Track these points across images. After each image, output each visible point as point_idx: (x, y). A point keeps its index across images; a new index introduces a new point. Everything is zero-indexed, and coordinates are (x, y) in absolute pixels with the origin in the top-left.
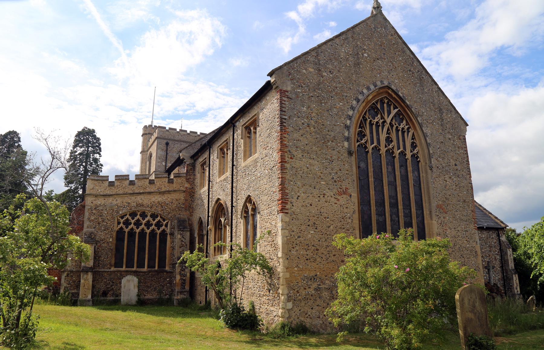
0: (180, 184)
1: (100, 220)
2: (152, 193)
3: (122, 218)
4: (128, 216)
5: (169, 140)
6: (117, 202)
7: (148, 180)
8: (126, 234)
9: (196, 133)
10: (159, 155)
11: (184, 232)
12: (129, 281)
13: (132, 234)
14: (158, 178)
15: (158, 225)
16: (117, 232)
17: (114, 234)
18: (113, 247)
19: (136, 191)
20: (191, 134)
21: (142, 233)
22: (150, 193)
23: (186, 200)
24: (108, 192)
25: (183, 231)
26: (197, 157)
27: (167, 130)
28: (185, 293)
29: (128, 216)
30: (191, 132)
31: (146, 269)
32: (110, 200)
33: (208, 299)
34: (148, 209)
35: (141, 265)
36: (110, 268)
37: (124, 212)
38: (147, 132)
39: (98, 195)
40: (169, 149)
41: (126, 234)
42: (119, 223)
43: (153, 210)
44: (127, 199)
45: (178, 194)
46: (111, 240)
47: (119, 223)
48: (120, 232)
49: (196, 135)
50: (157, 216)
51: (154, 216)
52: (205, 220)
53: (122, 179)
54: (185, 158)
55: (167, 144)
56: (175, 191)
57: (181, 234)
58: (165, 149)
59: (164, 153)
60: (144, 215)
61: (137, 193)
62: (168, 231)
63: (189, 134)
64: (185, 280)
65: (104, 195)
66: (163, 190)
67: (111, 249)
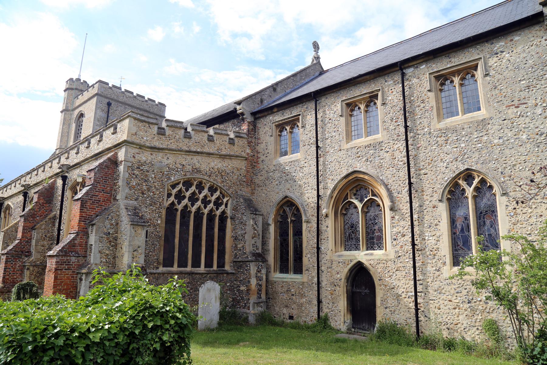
0: (241, 148)
1: (145, 188)
2: (212, 154)
3: (173, 186)
4: (181, 186)
5: (112, 99)
6: (169, 162)
7: (206, 134)
8: (179, 213)
9: (143, 97)
10: (97, 116)
11: (257, 216)
12: (209, 290)
13: (185, 212)
14: (219, 134)
15: (218, 203)
16: (168, 208)
17: (164, 212)
18: (162, 233)
19: (193, 149)
20: (138, 98)
21: (199, 215)
22: (209, 154)
23: (248, 172)
24: (157, 144)
25: (256, 214)
26: (266, 114)
27: (110, 88)
28: (262, 304)
29: (181, 186)
30: (138, 95)
31: (202, 269)
32: (159, 156)
33: (322, 314)
34: (207, 178)
35: (196, 263)
36: (158, 268)
37: (176, 178)
38: (74, 87)
39: (144, 146)
40: (110, 111)
41: (179, 213)
42: (169, 195)
43: (212, 180)
44: (182, 159)
45: (240, 162)
46: (159, 222)
47: (169, 195)
48: (171, 210)
49: (143, 100)
50: (216, 190)
51: (212, 190)
52: (308, 198)
53: (176, 127)
54: (245, 113)
55: (109, 104)
56: (237, 156)
57: (253, 219)
58: (106, 110)
59: (104, 115)
60: (200, 187)
61: (195, 152)
62: (229, 212)
63: (135, 97)
64: (261, 285)
65: (152, 148)
66: (223, 153)
67: (160, 237)
